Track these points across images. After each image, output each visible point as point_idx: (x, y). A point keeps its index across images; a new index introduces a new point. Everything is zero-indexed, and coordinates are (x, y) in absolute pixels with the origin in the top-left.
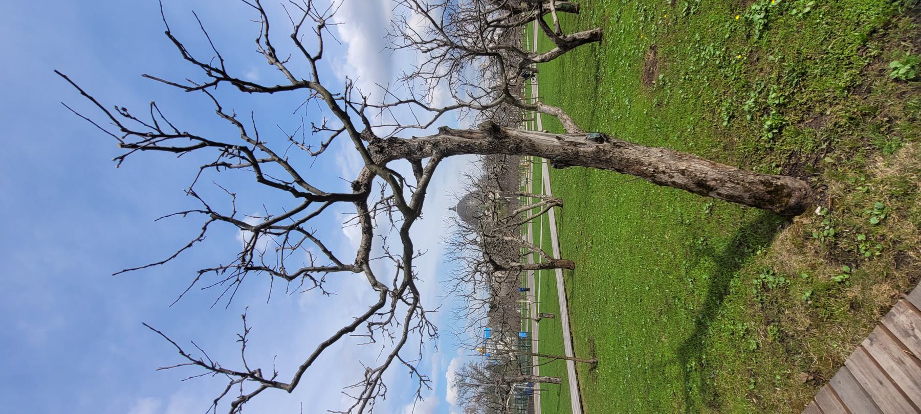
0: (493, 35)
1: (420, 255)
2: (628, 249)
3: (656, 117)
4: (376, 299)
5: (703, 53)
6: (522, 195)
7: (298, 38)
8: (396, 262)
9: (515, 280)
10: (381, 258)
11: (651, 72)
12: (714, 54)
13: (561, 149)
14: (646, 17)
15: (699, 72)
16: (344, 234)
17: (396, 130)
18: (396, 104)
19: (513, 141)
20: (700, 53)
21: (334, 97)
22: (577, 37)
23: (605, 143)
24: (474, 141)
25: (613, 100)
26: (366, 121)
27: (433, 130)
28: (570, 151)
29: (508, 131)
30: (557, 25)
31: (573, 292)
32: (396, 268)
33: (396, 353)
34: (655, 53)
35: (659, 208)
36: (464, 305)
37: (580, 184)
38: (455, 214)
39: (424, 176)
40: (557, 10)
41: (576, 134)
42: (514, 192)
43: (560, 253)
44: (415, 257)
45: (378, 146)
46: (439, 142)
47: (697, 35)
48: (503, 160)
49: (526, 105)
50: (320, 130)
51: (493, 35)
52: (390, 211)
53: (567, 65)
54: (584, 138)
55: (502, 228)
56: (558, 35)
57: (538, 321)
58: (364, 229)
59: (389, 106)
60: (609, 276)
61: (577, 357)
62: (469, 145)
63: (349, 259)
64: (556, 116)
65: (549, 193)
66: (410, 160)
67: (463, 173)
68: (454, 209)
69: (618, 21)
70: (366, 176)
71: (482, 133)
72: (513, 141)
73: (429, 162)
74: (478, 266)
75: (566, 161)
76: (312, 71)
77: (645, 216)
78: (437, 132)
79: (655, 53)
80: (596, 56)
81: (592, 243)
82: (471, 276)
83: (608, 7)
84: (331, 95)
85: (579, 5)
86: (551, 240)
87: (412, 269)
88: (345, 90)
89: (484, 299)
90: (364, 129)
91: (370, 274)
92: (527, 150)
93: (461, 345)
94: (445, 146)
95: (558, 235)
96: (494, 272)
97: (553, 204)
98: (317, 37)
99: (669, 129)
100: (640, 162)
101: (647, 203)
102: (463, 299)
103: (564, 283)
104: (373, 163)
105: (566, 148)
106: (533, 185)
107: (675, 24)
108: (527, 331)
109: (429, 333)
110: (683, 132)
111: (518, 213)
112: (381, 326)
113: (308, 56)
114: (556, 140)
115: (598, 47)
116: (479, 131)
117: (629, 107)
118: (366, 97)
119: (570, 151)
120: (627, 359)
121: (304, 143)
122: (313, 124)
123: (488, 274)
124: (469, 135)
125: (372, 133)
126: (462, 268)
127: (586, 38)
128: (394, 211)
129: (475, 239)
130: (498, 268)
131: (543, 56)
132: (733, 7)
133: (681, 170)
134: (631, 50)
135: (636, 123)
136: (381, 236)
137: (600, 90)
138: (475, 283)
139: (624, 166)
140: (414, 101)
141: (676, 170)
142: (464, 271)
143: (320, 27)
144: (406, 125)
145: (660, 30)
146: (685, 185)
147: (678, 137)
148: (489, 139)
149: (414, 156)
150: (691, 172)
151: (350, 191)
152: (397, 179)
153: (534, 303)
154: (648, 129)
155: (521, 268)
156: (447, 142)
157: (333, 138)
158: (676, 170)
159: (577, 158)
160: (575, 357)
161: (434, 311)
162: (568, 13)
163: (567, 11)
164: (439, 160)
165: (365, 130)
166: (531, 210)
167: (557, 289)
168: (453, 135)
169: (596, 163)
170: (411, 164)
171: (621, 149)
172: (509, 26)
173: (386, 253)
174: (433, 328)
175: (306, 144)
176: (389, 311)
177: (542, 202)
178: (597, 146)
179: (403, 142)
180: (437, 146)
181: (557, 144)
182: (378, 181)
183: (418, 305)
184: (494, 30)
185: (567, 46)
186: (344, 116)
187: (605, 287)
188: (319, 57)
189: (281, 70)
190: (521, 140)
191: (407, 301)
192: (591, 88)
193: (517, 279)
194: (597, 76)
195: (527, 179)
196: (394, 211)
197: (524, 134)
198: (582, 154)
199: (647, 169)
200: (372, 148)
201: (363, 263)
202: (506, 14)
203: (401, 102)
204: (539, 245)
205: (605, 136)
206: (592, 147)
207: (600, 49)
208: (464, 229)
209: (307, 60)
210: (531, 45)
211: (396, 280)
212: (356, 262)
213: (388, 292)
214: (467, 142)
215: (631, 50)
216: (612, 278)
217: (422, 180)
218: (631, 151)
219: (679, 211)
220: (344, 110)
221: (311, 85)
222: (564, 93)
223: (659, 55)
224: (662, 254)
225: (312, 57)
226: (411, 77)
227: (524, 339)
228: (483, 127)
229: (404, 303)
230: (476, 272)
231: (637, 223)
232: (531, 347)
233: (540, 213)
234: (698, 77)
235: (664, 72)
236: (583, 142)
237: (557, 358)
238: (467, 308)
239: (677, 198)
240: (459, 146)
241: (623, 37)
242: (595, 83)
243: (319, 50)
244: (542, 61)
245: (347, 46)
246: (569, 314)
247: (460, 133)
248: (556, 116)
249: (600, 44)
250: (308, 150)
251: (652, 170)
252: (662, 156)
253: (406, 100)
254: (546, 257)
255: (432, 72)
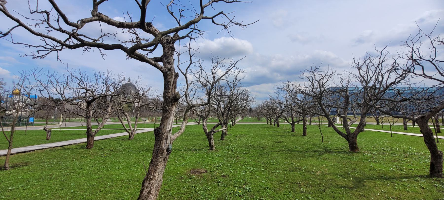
0: (215, 104)
1: (102, 55)
2: (101, 176)
3: (176, 178)
4: (73, 19)
5: (203, 192)
6: (137, 118)
7: (221, 15)
8: (98, 39)
9: (79, 114)
10: (101, 30)
11: (196, 172)
12: (202, 196)
13: (164, 132)
14: (218, 166)
15: (195, 192)
16: (115, 17)
17: (178, 53)
18: (190, 54)
19: (170, 108)
20: (203, 190)
21: (196, 24)
22: (212, 140)
23: (166, 153)
24: (171, 89)
25: (185, 158)
26: (183, 38)
27: (177, 70)
28: (163, 136)
29: (175, 106)
30: (217, 131)
31: (69, 149)
32: (94, 38)
33: (21, 25)
34: (204, 173)
35: (127, 188)
36: (59, 81)
37: (142, 147)
38: (126, 82)
39: (153, 62)
40: (223, 131)
41: (171, 139)
42: (139, 113)
43: (98, 140)
44: (100, 51)
45: (170, 41)
46: (171, 72)
47: (210, 188)
48: (157, 108)
49: (186, 115)
50: (180, 13)
51: (215, 104)
52: (132, 42)
53: (201, 137)
54: (169, 143)
55: (117, 106)
56: (213, 132)
57: (45, 129)
58: (123, 23)
59: (190, 51)
60: (81, 169)
61: (11, 156)
62: (169, 87)
63: (101, 9)
64: (181, 129)
65: (137, 132)
66: (162, 56)
67: (151, 87)
68: (129, 81)
69: (217, 156)
70: (155, 31)
71: (174, 93)
72: (170, 108)
73: (161, 66)
74: (90, 91)
75: (158, 135)
76: (208, 17)
77: (122, 182)
78: (176, 72)
79: (204, 173)
80: (204, 148)
81: (105, 157)
82: (83, 86)
83: (222, 151)
84: (197, 22)
85: (224, 140)
86: (107, 134)
87: (92, 48)
88: (199, 30)
89: (65, 94)
90: (179, 36)
91: (91, 21)
92: (165, 115)
93: (24, 76)
94: (169, 75)
95: (110, 138)
96: (86, 101)
97: (131, 134)
98: (221, 24)
99: (170, 184)
100: (156, 171)
101: (130, 182)
102: (65, 81)
103: (76, 144)
104: (163, 35)
105: (165, 135)
106: (142, 124)
107: (215, 178)
108: (34, 123)
109: (41, 50)
110: (168, 191)
111: (126, 115)
112: (47, 20)
113: (214, 17)
114: (169, 129)
115: (207, 149)
116: (175, 92)
117: (181, 165)
118: (195, 39)
119: (163, 136)
120: (10, 188)
121: (173, 3)
122: (184, 11)
123: (84, 97)
124: (174, 87)
125: (177, 39)
126: (89, 82)
127: (211, 144)
128: (132, 44)
129: (109, 91)
130: (89, 103)
131: (205, 126)
132: (220, 199)
133: (151, 191)
134: (205, 162)
135: (174, 170)
136: (117, 33)
137: (189, 152)
138: (78, 89)
139: (153, 164)
140: (191, 63)
141: (150, 189)
142: (87, 83)
143: (225, 26)
144: (180, 58)
145: (213, 173)
146: (142, 195)
147: (166, 189)
148: (171, 97)
149: (165, 59)
150: (149, 196)
151: (147, 21)
152: (152, 48)
153: (60, 127)
154: (170, 175)
155: (88, 117)
156: (171, 76)
157: (176, 19)
158: (150, 189)
159: (159, 140)
160: (11, 155)
161: (58, 58)
162: (221, 136)
163: (222, 135)
164: (162, 71)
165: (179, 36)
166: (127, 123)
167: (71, 140)
168: (174, 79)
169: (156, 150)
170: (160, 56)
171: (163, 161)
172: (218, 111)
173: (104, 34)
174: (43, 56)
175: (173, 5)
176: (60, 27)
177: (132, 129)
178: (165, 149)
179: (172, 54)
180: (169, 71)
181: (167, 130)
182: (151, 37)
183: (64, 47)
184: (217, 105)
185: (209, 136)
186: (187, 27)
187: (73, 167)
188: (213, 22)
189: (209, 2)
190: (170, 112)
191: (68, 41)
192: (190, 148)
193: (79, 115)
194: (195, 150)
195: (146, 121)
196: (132, 44)
197: (173, 114)
198: (161, 142)
199: (152, 175)
200: (169, 38)
201: (100, 18)
202: (223, 110)
203: (191, 57)
204: (104, 128)
205: (170, 152)
206: (165, 147)
207: (207, 150)
208: (117, 85)
209: (212, 16)
210: (209, 122)
211: (85, 36)
212: (99, 13)
213: (76, 29)
214: (170, 86)
215: (205, 162)
216: (80, 170)
217: (151, 61)
218: (162, 166)
219: (126, 198)
220: (190, 27)
221: (202, 15)
222: (188, 136)
223: (203, 174)
224: (97, 195)
225: (213, 18)
226: (200, 66)
227: (28, 121)
228: (178, 94)
229: (66, 39)
230: (86, 90)
231: (118, 179)
232: (19, 125)
233: (125, 127)
234: (193, 192)
235: (196, 177)
236: (168, 142)
237: (10, 142)
238: (57, 83)
239: (133, 195)
240: (169, 82)
241: (211, 158)
242: (192, 149)
243: (216, 23)
244: (203, 125)
245: (212, 40)
246: (51, 148)
247: (175, 83)
248: (181, 129)
249: (209, 150)
250: (170, 5)
251: (151, 178)
252: (158, 181)
253: (192, 59)
254: (96, 131)
255: (202, 76)
